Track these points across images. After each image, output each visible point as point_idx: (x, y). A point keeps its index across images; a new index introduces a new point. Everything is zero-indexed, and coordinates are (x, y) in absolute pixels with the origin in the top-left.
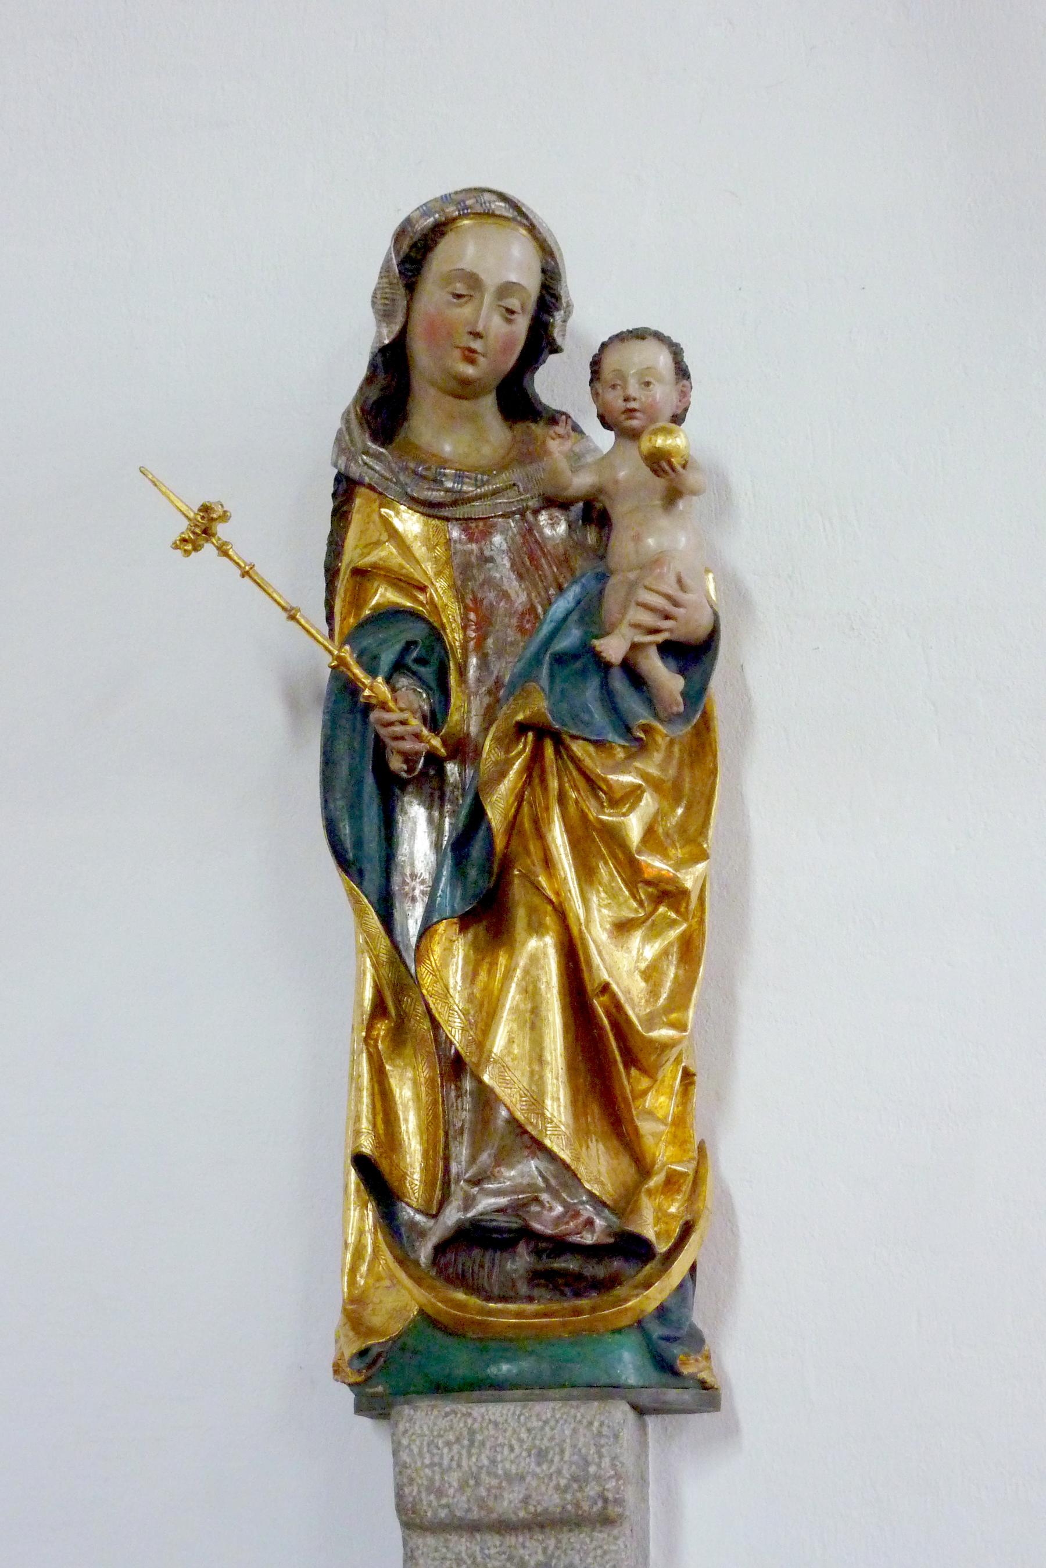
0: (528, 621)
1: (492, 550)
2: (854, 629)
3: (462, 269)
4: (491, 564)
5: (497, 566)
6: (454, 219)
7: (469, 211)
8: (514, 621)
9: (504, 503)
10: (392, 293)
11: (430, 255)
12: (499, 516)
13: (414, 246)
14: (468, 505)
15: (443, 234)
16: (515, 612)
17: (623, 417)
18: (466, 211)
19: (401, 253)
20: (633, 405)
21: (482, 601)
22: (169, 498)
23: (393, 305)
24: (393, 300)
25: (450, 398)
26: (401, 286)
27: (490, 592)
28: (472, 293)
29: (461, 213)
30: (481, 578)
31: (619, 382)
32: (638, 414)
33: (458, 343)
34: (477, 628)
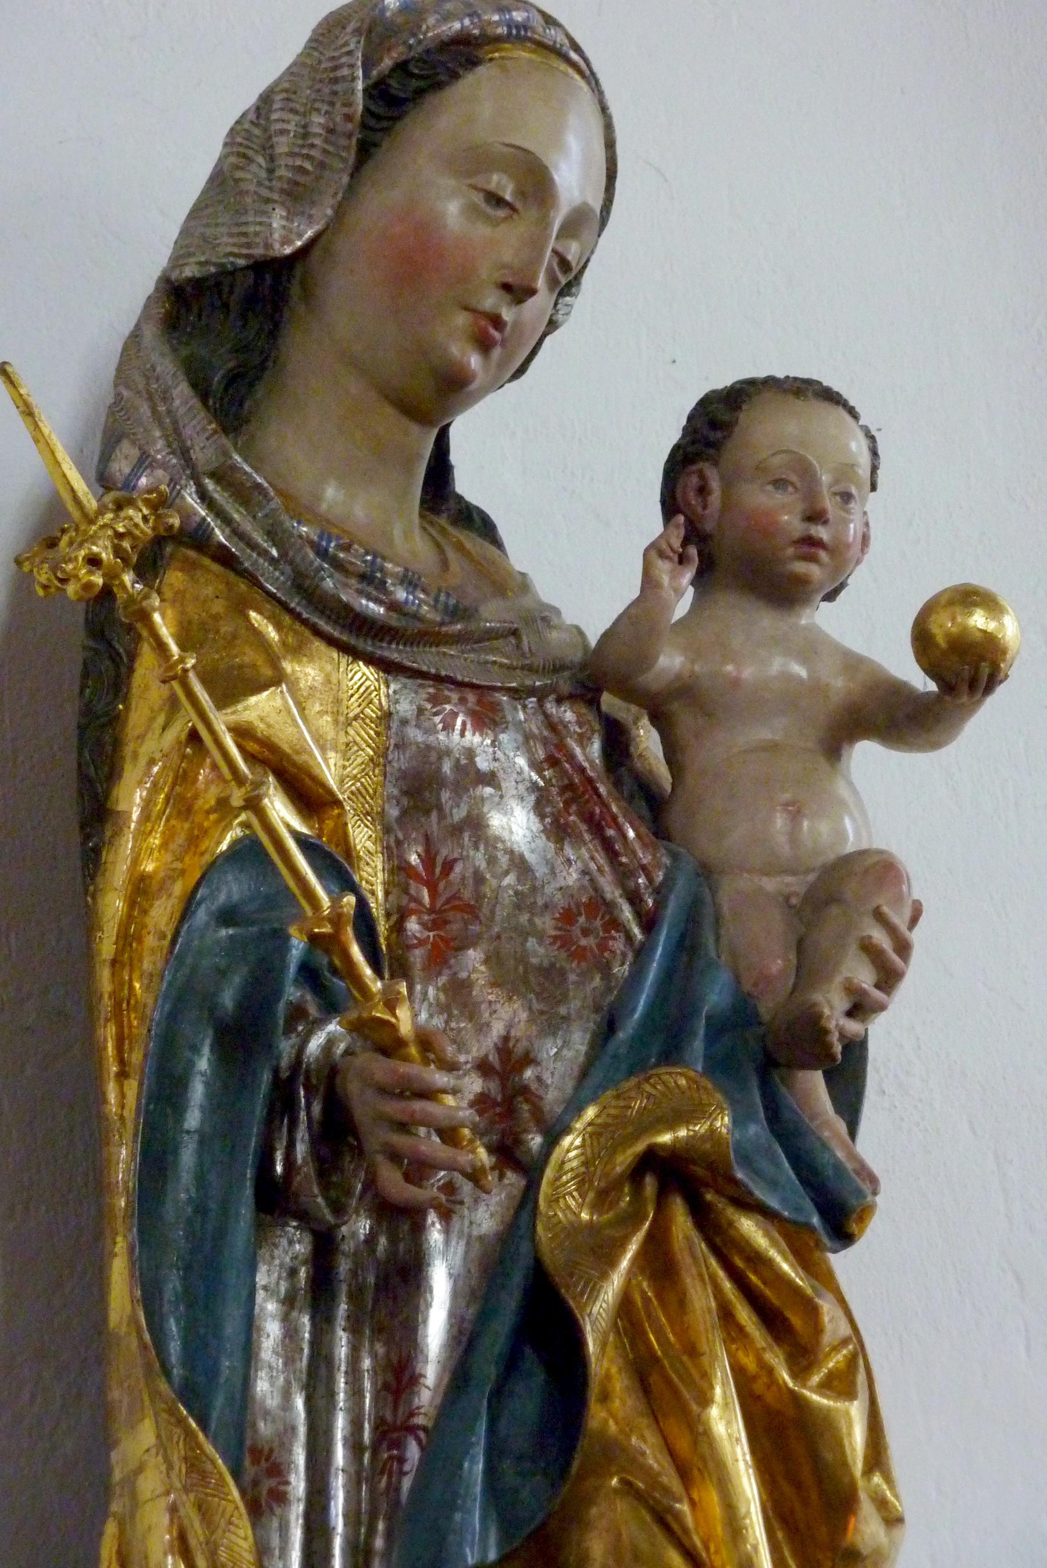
0: (586, 932)
1: (495, 760)
2: (884, 1092)
3: (525, 150)
4: (488, 790)
5: (501, 797)
6: (498, 39)
7: (529, 34)
8: (546, 923)
9: (502, 665)
10: (325, 151)
11: (432, 100)
12: (509, 690)
13: (401, 67)
14: (434, 649)
15: (473, 63)
16: (546, 906)
17: (790, 551)
18: (523, 33)
19: (375, 73)
20: (822, 533)
21: (448, 866)
22: (53, 453)
23: (318, 178)
24: (322, 165)
25: (389, 410)
26: (354, 141)
27: (477, 849)
28: (518, 205)
29: (514, 32)
30: (459, 814)
31: (794, 478)
32: (823, 555)
33: (473, 303)
34: (434, 921)
